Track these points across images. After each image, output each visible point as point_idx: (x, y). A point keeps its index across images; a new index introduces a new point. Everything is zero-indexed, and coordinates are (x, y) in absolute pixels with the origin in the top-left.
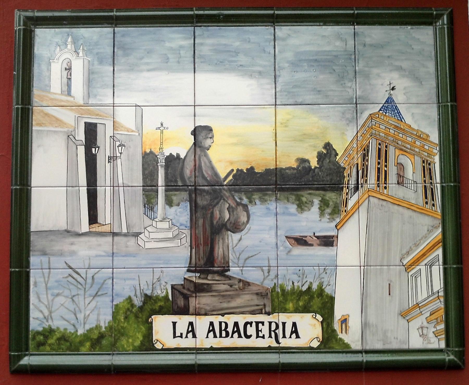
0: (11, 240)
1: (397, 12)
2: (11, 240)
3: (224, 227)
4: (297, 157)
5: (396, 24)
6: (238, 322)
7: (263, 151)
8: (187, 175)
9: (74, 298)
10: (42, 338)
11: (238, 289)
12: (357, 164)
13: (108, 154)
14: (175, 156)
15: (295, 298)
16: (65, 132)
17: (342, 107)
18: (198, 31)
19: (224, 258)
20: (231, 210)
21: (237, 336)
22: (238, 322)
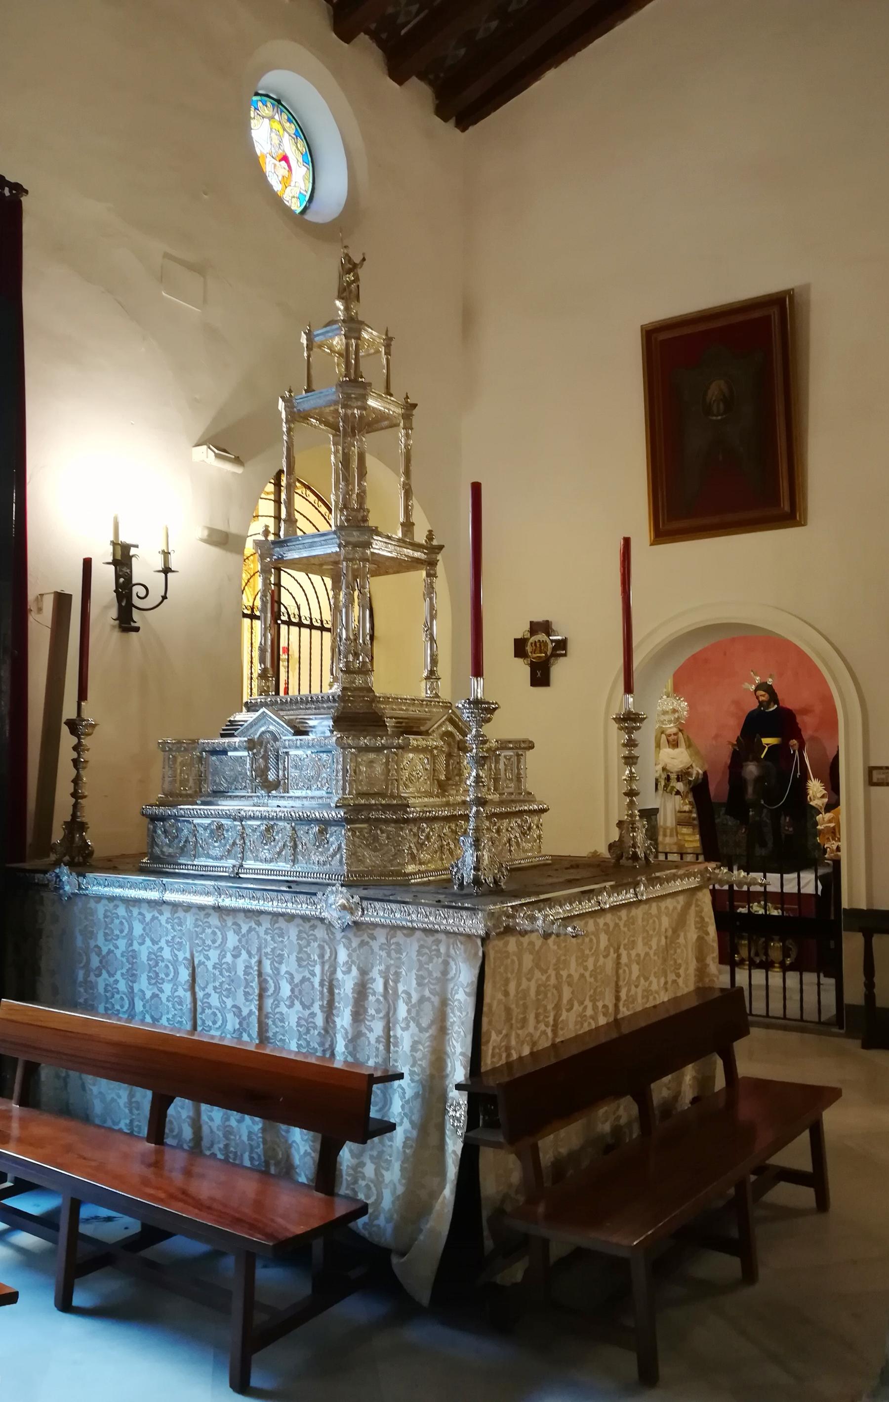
0: (251, 689)
2: (251, 689)
3: (359, 1169)
4: (447, 130)
5: (865, 957)
6: (91, 559)
7: (126, 1228)
8: (486, 1064)
9: (875, 780)
10: (98, 964)
11: (227, 1123)
12: (166, 256)
13: (401, 520)
14: (608, 855)
15: (382, 832)
17: (99, 1170)
18: (249, 1041)
19: (334, 701)
20: (446, 885)
21: (660, 817)
22: (91, 559)
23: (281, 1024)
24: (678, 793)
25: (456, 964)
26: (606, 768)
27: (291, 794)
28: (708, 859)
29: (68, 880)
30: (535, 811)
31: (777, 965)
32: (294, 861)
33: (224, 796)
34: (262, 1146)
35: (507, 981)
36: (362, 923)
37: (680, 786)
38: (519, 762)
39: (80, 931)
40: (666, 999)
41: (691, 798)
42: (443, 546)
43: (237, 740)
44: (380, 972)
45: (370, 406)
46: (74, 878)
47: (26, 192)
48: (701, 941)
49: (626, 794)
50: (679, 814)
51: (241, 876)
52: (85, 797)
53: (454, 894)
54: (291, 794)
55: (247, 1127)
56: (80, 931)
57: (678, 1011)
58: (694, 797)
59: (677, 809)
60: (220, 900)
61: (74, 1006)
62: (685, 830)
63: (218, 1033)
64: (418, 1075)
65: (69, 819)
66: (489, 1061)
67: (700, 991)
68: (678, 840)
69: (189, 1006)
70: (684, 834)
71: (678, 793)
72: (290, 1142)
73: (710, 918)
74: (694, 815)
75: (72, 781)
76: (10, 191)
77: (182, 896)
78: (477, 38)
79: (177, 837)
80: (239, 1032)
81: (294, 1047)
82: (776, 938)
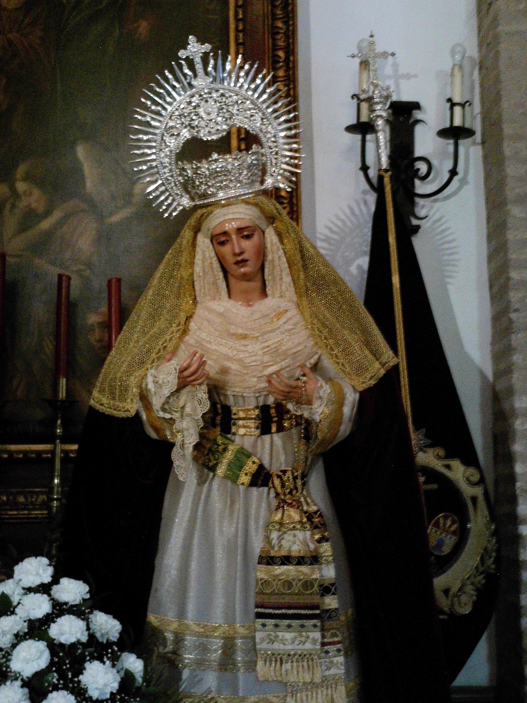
1: (64, 294)
16: (246, 492)
22: (420, 227)
23: (295, 660)
24: (261, 478)
29: (221, 391)
31: (82, 697)
32: (244, 407)
33: (206, 218)
35: (283, 486)
36: (169, 247)
37: (275, 451)
38: (309, 469)
41: (316, 494)
43: (148, 179)
45: (75, 153)
46: (219, 433)
47: (416, 106)
48: (154, 317)
49: (350, 129)
50: (262, 572)
55: (246, 192)
59: (257, 546)
62: (288, 639)
63: (197, 183)
64: (331, 556)
66: (447, 609)
68: (275, 632)
70: (279, 659)
71: (261, 478)
72: (390, 111)
74: (329, 572)
76: (80, 698)
82: (58, 504)
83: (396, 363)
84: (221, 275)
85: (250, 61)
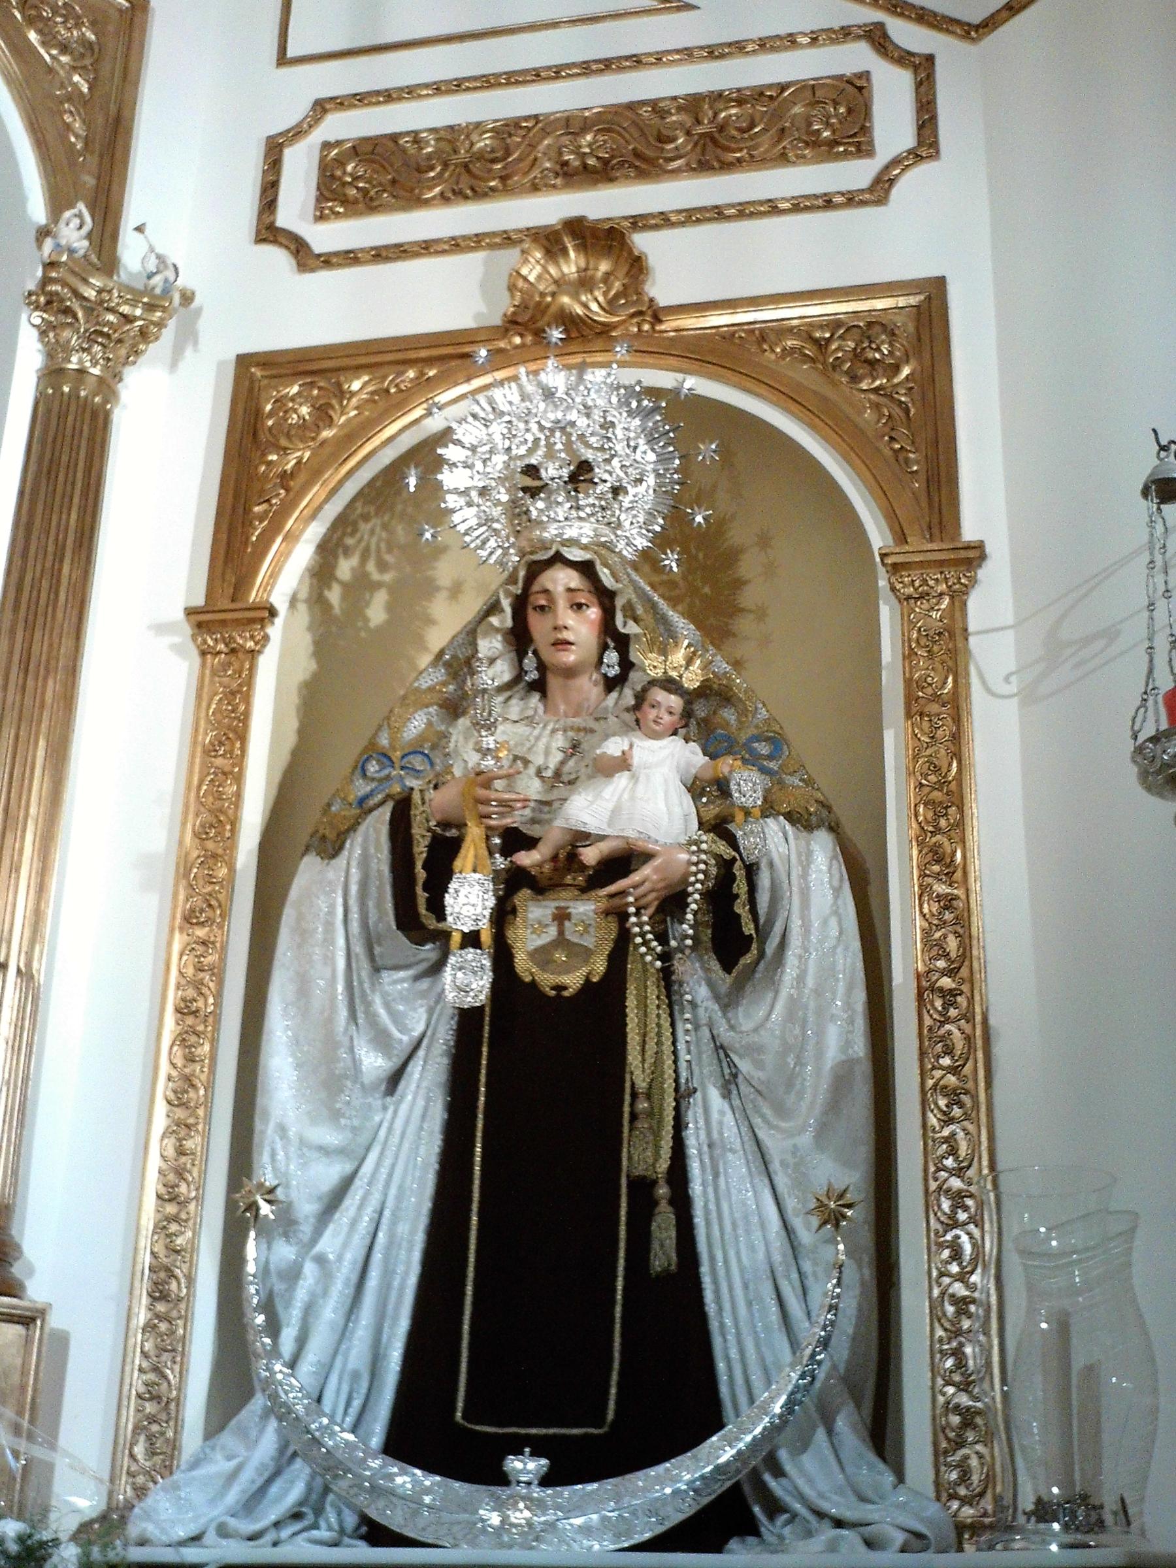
25: (942, 1223)
26: (637, 61)
27: (177, 935)
28: (627, 636)
30: (755, 1327)
34: (651, 480)
39: (515, 583)
40: (413, 831)
42: (144, 224)
44: (427, 143)
51: (485, 528)
52: (830, 1184)
53: (568, 1545)
54: (177, 935)
56: (515, 583)
57: (459, 1487)
58: (495, 951)
60: (395, 1052)
61: (654, 393)
65: (189, 352)
67: (582, 368)
69: (690, 1113)
72: (590, 252)
73: (633, 1039)
75: (260, 240)
77: (671, 1118)
78: (413, 472)
79: (586, 569)
80: (669, 1265)
81: (182, 1534)
83: (430, 646)
84: (929, 1375)
85: (247, 1231)
